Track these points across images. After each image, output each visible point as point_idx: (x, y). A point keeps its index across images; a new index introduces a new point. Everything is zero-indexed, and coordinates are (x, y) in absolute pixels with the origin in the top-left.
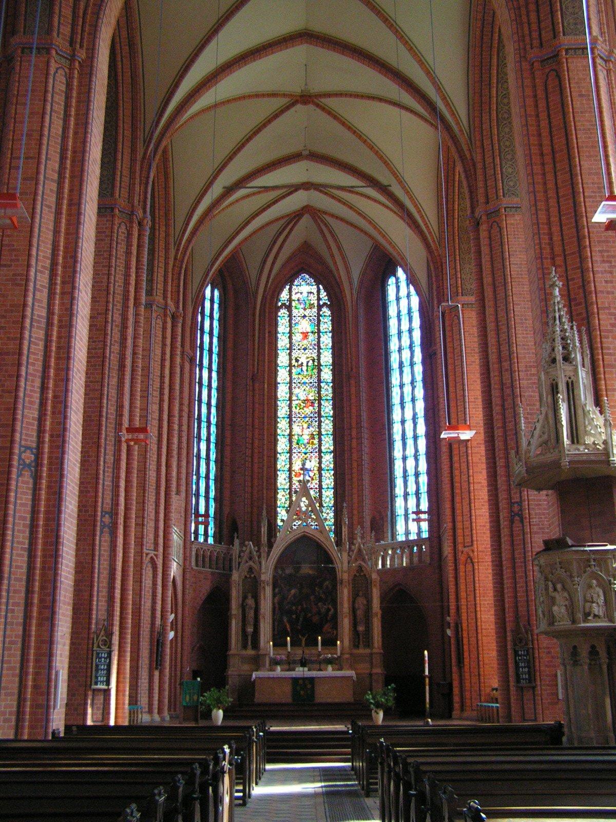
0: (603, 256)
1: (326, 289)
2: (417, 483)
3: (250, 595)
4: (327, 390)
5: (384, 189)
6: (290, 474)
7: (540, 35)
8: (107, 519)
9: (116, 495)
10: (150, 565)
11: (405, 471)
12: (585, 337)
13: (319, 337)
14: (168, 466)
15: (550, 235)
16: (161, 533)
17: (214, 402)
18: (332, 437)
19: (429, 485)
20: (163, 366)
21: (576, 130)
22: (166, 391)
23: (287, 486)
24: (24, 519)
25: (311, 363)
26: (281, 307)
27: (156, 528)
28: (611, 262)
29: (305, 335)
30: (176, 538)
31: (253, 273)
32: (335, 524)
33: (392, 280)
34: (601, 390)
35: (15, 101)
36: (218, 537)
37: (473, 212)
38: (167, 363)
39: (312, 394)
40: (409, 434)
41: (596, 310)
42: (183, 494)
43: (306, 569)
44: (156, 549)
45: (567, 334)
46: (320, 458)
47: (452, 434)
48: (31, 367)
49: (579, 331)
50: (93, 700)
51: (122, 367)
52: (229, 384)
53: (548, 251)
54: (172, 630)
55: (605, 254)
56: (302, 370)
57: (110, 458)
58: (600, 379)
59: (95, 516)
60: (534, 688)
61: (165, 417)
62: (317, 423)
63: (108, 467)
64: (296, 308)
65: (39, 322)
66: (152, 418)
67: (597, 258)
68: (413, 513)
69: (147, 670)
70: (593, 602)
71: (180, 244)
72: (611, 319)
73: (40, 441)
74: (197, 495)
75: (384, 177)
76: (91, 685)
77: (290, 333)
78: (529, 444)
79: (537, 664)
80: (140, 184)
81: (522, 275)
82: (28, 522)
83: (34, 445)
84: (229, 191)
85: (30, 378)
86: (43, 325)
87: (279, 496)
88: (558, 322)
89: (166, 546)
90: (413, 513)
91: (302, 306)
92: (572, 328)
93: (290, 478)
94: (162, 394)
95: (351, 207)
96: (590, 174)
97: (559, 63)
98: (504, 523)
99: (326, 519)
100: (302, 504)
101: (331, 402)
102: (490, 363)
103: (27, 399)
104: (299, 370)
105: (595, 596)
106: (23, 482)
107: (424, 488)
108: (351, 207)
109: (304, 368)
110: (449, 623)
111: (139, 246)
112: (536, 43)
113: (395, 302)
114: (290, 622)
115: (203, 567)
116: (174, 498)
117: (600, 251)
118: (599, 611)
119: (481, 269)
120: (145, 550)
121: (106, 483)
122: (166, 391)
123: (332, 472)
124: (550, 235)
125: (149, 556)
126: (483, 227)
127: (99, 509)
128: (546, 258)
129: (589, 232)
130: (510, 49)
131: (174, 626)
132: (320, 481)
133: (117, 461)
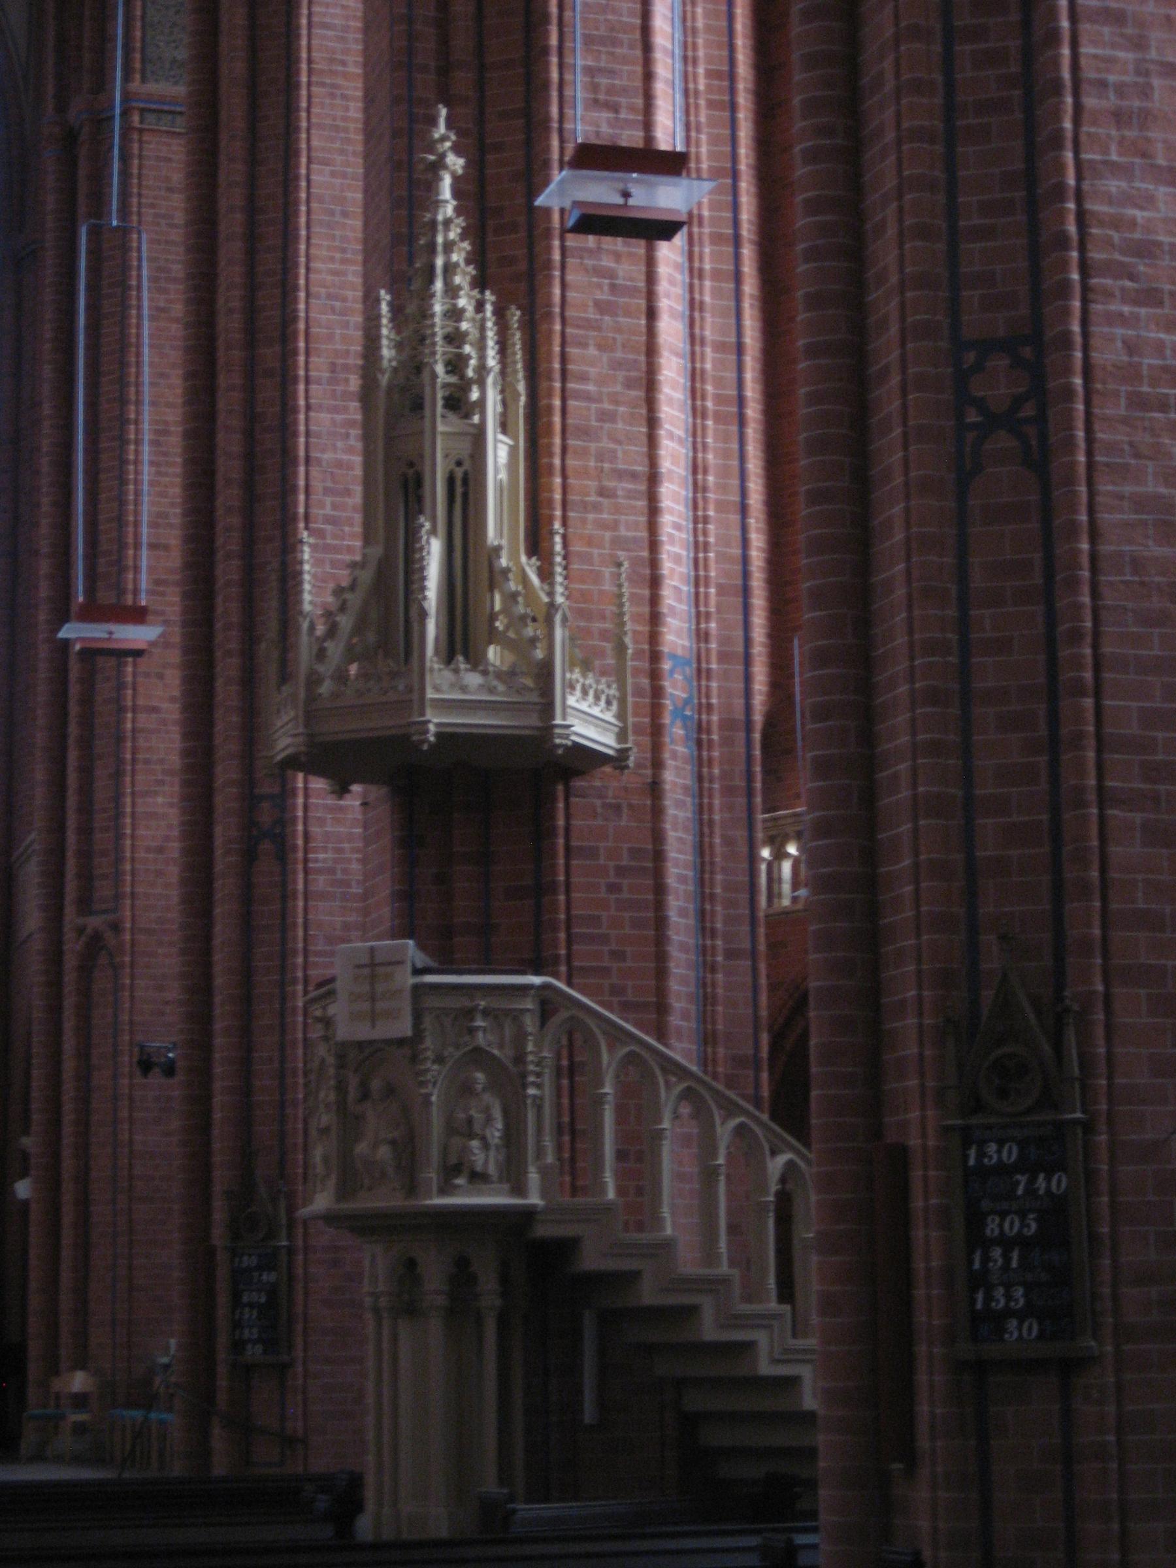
12: (517, 338)
28: (615, 108)
41: (557, 256)
45: (464, 326)
49: (500, 313)
55: (604, 81)
60: (283, 1369)
67: (579, 91)
70: (471, 1136)
72: (600, 286)
78: (321, 654)
79: (299, 1297)
81: (344, 63)
88: (439, 285)
92: (480, 307)
98: (224, 861)
102: (221, 343)
105: (478, 1116)
110: (25, 1156)
118: (486, 1162)
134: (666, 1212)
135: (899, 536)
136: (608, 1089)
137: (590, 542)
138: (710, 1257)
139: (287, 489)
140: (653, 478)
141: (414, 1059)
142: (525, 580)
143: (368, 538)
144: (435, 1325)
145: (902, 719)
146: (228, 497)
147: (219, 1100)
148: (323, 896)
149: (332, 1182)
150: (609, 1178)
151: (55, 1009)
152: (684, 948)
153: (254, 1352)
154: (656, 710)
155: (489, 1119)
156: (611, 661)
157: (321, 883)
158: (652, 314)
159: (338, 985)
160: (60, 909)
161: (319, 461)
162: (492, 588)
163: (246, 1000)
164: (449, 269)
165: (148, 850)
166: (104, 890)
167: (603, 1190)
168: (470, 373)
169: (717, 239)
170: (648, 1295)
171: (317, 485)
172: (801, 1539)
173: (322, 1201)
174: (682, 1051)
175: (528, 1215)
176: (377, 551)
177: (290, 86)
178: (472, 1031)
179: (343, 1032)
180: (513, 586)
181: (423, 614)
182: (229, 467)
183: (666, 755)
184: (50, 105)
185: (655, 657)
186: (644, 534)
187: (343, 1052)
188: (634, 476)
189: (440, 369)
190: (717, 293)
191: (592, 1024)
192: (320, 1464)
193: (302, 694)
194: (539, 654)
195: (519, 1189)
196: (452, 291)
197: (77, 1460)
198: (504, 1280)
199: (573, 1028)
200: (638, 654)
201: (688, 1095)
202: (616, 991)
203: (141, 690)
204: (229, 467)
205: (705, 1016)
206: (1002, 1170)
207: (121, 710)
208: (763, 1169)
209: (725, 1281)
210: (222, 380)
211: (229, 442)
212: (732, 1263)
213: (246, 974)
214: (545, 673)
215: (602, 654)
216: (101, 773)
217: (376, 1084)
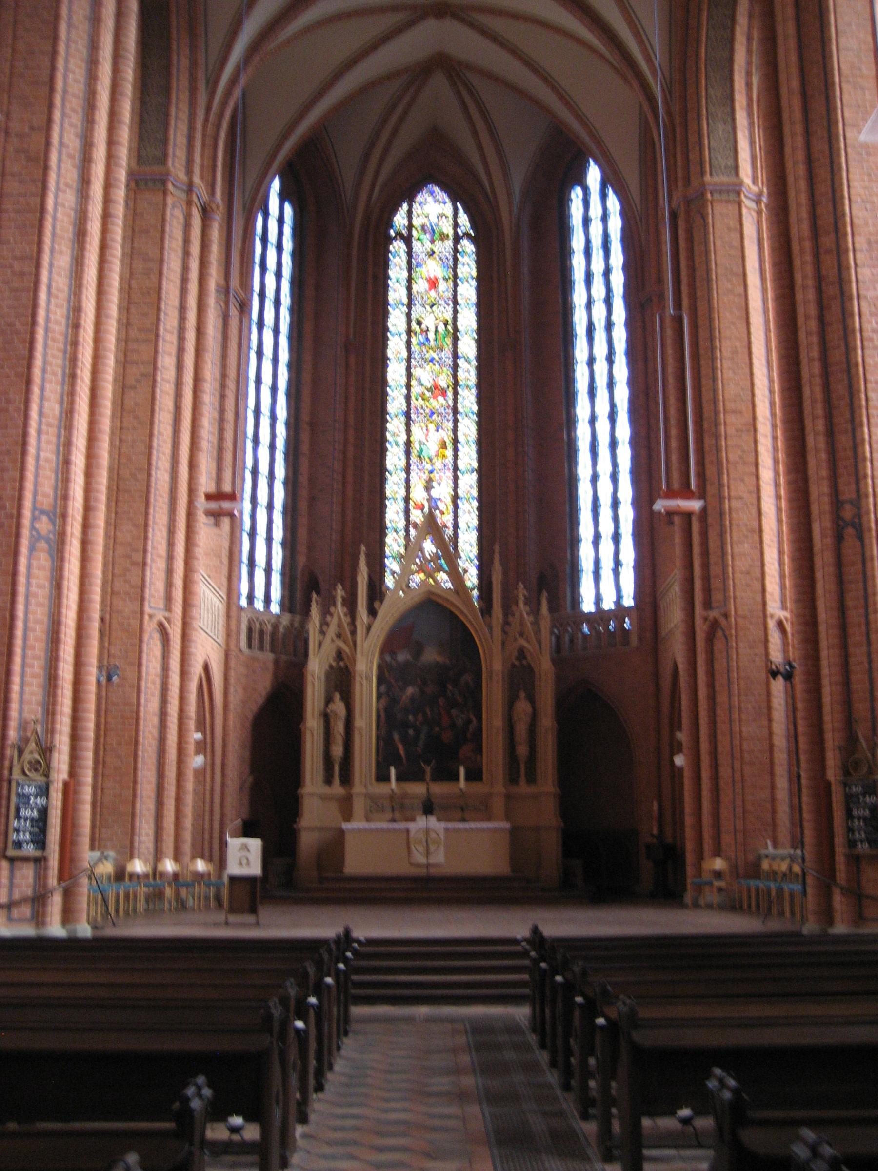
2: (616, 519)
3: (337, 696)
4: (468, 371)
8: (44, 525)
9: (65, 479)
10: (157, 636)
13: (456, 285)
14: (193, 466)
16: (178, 582)
20: (184, 291)
25: (441, 328)
27: (170, 572)
29: (433, 284)
31: (347, 174)
33: (577, 194)
36: (287, 604)
43: (431, 655)
44: (168, 607)
46: (456, 478)
51: (81, 234)
52: (308, 357)
54: (197, 752)
56: (427, 339)
57: (53, 408)
59: (19, 515)
63: (49, 425)
66: (163, 379)
69: (152, 820)
76: (700, 857)
77: (410, 280)
87: (389, 540)
93: (407, 512)
94: (181, 339)
95: (514, 52)
108: (514, 52)
109: (431, 336)
110: (680, 744)
114: (404, 740)
120: (147, 609)
121: (42, 454)
127: (28, 504)
131: (201, 747)
133: (68, 414)
161: (866, 297)
165: (741, 572)
166: (717, 596)
203: (732, 487)
206: (857, 795)
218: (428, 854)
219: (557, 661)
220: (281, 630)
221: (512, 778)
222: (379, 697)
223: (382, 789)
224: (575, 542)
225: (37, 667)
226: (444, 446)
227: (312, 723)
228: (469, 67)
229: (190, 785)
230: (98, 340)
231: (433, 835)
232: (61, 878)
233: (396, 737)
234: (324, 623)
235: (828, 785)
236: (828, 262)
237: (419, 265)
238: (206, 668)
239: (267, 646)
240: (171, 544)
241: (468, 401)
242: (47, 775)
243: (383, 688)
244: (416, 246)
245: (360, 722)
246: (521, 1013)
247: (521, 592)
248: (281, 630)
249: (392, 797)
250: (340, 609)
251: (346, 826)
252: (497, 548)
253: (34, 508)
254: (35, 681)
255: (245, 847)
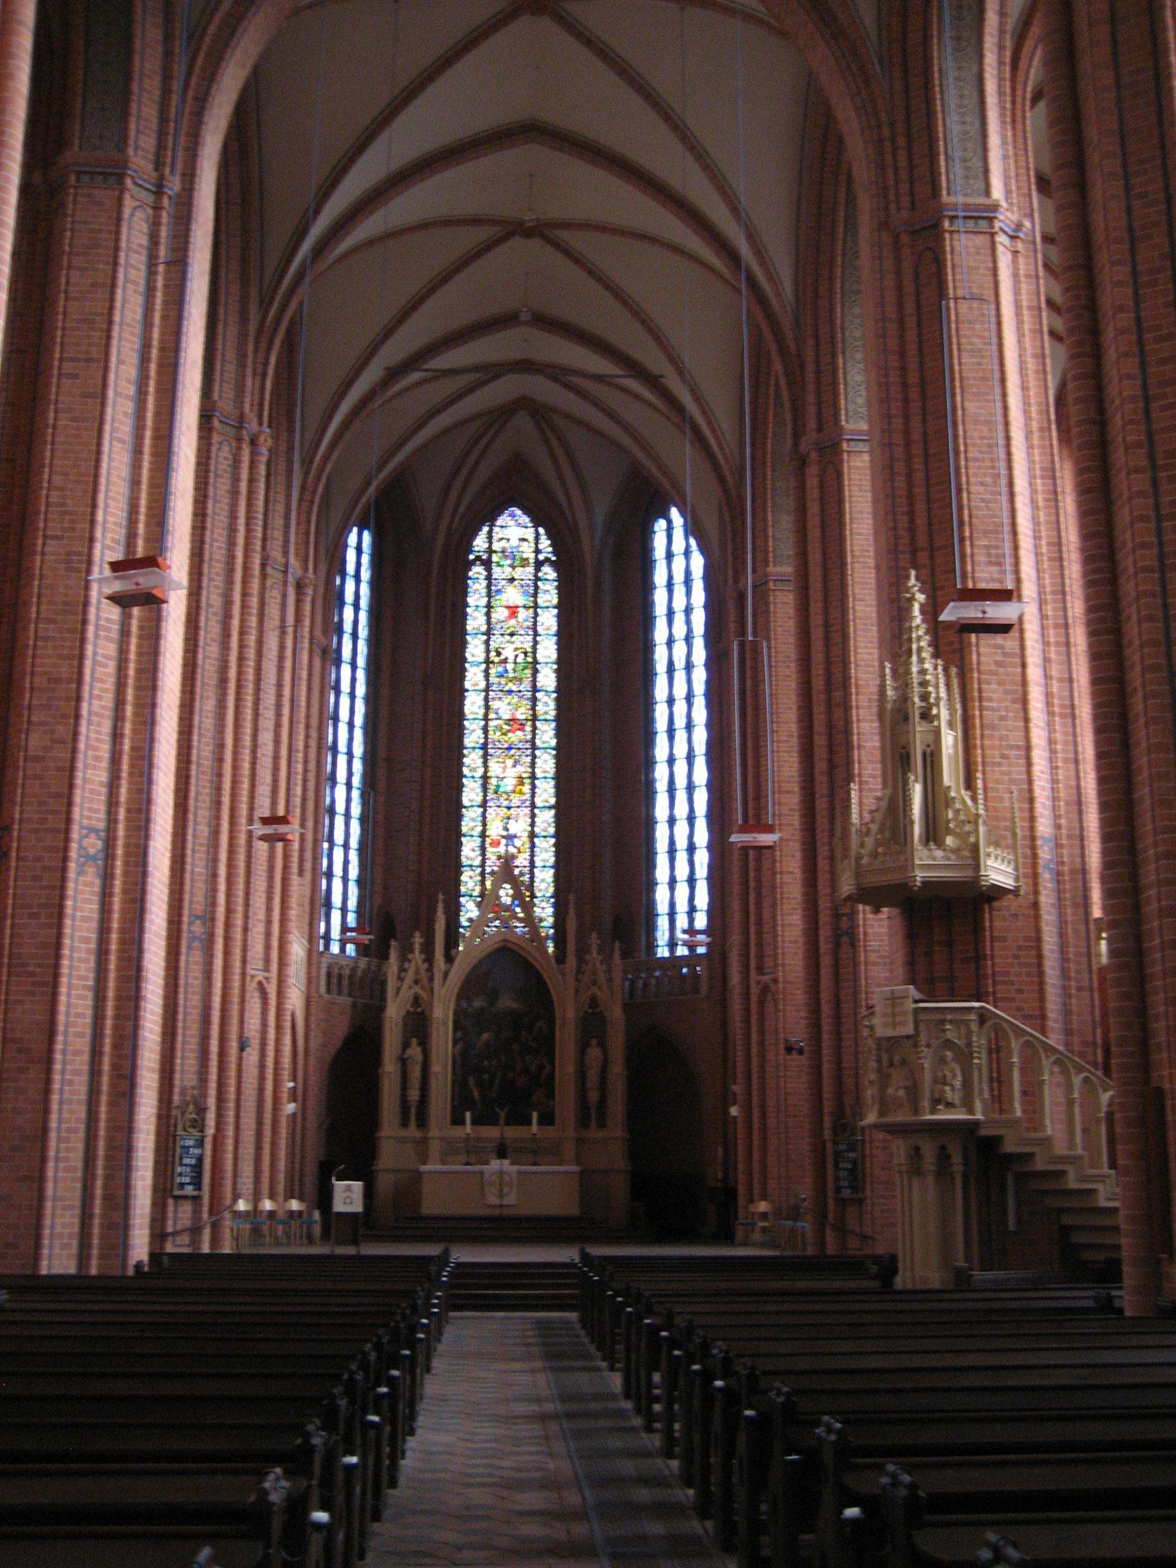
0: (989, 555)
1: (550, 536)
3: (414, 1041)
4: (546, 704)
5: (653, 382)
6: (483, 842)
7: (912, 188)
8: (198, 928)
10: (257, 994)
11: (672, 843)
12: (955, 682)
13: (536, 615)
15: (911, 514)
16: (275, 943)
17: (359, 720)
18: (552, 783)
19: (710, 867)
21: (959, 350)
22: (286, 710)
23: (477, 862)
24: (86, 940)
26: (473, 563)
27: (268, 935)
29: (513, 611)
30: (297, 949)
32: (555, 926)
33: (661, 525)
34: (975, 763)
35: (65, 263)
37: (796, 444)
38: (288, 664)
39: (522, 710)
40: (681, 782)
42: (308, 876)
43: (507, 1002)
44: (267, 969)
46: (533, 816)
47: (746, 838)
48: (96, 702)
49: (946, 670)
50: (176, 1211)
51: (223, 681)
53: (906, 541)
55: (994, 552)
56: (506, 671)
58: (975, 746)
60: (861, 1201)
61: (284, 752)
62: (529, 759)
64: (498, 565)
65: (107, 629)
67: (981, 558)
68: (684, 932)
69: (252, 1163)
70: (945, 1084)
71: (311, 462)
73: (112, 820)
74: (329, 875)
75: (656, 363)
77: (489, 606)
78: (862, 845)
80: (254, 375)
82: (93, 946)
83: (102, 825)
84: (393, 374)
85: (95, 719)
86: (115, 635)
88: (914, 658)
89: (282, 964)
90: (684, 932)
91: (509, 562)
92: (936, 668)
93: (483, 849)
96: (976, 422)
97: (940, 240)
98: (825, 947)
99: (541, 920)
100: (502, 893)
101: (553, 725)
103: (90, 753)
104: (500, 669)
106: (86, 884)
107: (702, 872)
109: (510, 667)
111: (251, 480)
112: (905, 201)
113: (664, 562)
115: (339, 994)
116: (295, 879)
117: (987, 547)
119: (805, 536)
122: (286, 710)
123: (553, 841)
124: (911, 514)
125: (256, 980)
126: (813, 470)
127: (186, 912)
128: (903, 552)
129: (970, 516)
130: (866, 205)
131: (293, 1097)
132: (532, 855)
133: (216, 833)
134: (1048, 1122)
135: (1146, 774)
136: (1015, 1060)
137: (997, 782)
138: (1071, 1144)
139: (849, 763)
140: (1028, 748)
141: (915, 1045)
142: (964, 803)
143: (885, 784)
144: (930, 1181)
145: (1152, 867)
146: (821, 767)
147: (826, 1067)
148: (874, 964)
149: (876, 1108)
150: (1017, 1105)
151: (747, 1022)
152: (1054, 986)
153: (847, 1193)
154: (1035, 865)
155: (954, 1076)
156: (1010, 842)
157: (873, 957)
158: (1024, 666)
159: (877, 1009)
160: (748, 972)
162: (947, 806)
163: (837, 1019)
164: (920, 650)
166: (768, 962)
167: (1013, 1110)
168: (932, 700)
169: (1056, 626)
170: (1040, 1165)
171: (864, 758)
172: (1114, 1293)
173: (871, 1118)
174: (1055, 1040)
175: (976, 1124)
176: (889, 791)
177: (843, 565)
178: (944, 1031)
179: (881, 1032)
180: (958, 806)
181: (912, 822)
182: (820, 752)
183: (1041, 888)
184: (730, 583)
185: (1033, 838)
186: (1024, 777)
187: (880, 1042)
188: (1018, 747)
189: (916, 699)
190: (1058, 653)
191: (1005, 1026)
192: (881, 1250)
193: (853, 863)
194: (972, 839)
195: (971, 1111)
196: (921, 661)
197: (763, 1245)
198: (966, 1158)
199: (997, 1029)
200: (1024, 838)
201: (1057, 1062)
202: (1019, 1009)
204: (820, 752)
205: (1067, 1022)
207: (775, 874)
208: (1097, 1098)
209: (1079, 1158)
210: (816, 710)
211: (820, 741)
212: (1084, 1149)
213: (837, 1002)
214: (975, 848)
215: (1005, 838)
216: (767, 903)
217: (896, 1058)
218: (501, 1195)
219: (626, 1007)
220: (359, 973)
221: (583, 1121)
222: (455, 1042)
223: (457, 1132)
224: (652, 884)
225: (194, 1043)
226: (521, 780)
227: (390, 1067)
228: (554, 410)
229: (283, 1132)
230: (236, 767)
231: (506, 1178)
232: (211, 1213)
233: (471, 1081)
234: (402, 969)
235: (824, 1142)
236: (838, 713)
237: (499, 591)
238: (293, 1015)
239: (345, 990)
240: (269, 909)
241: (547, 735)
242: (202, 1131)
243: (459, 1034)
244: (497, 572)
245: (436, 1068)
246: (573, 1316)
247: (594, 939)
248: (359, 973)
249: (467, 1139)
250: (417, 956)
251: (424, 1168)
252: (572, 897)
253: (191, 915)
254: (193, 1055)
255: (348, 1188)
